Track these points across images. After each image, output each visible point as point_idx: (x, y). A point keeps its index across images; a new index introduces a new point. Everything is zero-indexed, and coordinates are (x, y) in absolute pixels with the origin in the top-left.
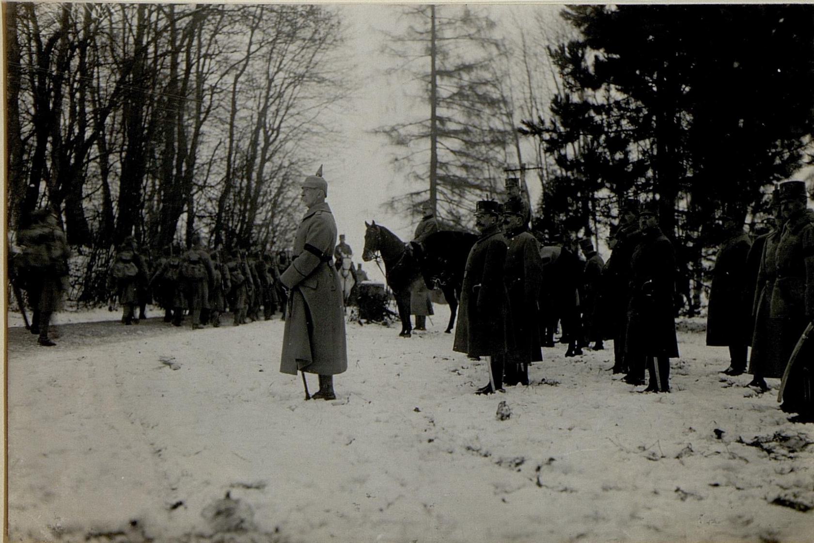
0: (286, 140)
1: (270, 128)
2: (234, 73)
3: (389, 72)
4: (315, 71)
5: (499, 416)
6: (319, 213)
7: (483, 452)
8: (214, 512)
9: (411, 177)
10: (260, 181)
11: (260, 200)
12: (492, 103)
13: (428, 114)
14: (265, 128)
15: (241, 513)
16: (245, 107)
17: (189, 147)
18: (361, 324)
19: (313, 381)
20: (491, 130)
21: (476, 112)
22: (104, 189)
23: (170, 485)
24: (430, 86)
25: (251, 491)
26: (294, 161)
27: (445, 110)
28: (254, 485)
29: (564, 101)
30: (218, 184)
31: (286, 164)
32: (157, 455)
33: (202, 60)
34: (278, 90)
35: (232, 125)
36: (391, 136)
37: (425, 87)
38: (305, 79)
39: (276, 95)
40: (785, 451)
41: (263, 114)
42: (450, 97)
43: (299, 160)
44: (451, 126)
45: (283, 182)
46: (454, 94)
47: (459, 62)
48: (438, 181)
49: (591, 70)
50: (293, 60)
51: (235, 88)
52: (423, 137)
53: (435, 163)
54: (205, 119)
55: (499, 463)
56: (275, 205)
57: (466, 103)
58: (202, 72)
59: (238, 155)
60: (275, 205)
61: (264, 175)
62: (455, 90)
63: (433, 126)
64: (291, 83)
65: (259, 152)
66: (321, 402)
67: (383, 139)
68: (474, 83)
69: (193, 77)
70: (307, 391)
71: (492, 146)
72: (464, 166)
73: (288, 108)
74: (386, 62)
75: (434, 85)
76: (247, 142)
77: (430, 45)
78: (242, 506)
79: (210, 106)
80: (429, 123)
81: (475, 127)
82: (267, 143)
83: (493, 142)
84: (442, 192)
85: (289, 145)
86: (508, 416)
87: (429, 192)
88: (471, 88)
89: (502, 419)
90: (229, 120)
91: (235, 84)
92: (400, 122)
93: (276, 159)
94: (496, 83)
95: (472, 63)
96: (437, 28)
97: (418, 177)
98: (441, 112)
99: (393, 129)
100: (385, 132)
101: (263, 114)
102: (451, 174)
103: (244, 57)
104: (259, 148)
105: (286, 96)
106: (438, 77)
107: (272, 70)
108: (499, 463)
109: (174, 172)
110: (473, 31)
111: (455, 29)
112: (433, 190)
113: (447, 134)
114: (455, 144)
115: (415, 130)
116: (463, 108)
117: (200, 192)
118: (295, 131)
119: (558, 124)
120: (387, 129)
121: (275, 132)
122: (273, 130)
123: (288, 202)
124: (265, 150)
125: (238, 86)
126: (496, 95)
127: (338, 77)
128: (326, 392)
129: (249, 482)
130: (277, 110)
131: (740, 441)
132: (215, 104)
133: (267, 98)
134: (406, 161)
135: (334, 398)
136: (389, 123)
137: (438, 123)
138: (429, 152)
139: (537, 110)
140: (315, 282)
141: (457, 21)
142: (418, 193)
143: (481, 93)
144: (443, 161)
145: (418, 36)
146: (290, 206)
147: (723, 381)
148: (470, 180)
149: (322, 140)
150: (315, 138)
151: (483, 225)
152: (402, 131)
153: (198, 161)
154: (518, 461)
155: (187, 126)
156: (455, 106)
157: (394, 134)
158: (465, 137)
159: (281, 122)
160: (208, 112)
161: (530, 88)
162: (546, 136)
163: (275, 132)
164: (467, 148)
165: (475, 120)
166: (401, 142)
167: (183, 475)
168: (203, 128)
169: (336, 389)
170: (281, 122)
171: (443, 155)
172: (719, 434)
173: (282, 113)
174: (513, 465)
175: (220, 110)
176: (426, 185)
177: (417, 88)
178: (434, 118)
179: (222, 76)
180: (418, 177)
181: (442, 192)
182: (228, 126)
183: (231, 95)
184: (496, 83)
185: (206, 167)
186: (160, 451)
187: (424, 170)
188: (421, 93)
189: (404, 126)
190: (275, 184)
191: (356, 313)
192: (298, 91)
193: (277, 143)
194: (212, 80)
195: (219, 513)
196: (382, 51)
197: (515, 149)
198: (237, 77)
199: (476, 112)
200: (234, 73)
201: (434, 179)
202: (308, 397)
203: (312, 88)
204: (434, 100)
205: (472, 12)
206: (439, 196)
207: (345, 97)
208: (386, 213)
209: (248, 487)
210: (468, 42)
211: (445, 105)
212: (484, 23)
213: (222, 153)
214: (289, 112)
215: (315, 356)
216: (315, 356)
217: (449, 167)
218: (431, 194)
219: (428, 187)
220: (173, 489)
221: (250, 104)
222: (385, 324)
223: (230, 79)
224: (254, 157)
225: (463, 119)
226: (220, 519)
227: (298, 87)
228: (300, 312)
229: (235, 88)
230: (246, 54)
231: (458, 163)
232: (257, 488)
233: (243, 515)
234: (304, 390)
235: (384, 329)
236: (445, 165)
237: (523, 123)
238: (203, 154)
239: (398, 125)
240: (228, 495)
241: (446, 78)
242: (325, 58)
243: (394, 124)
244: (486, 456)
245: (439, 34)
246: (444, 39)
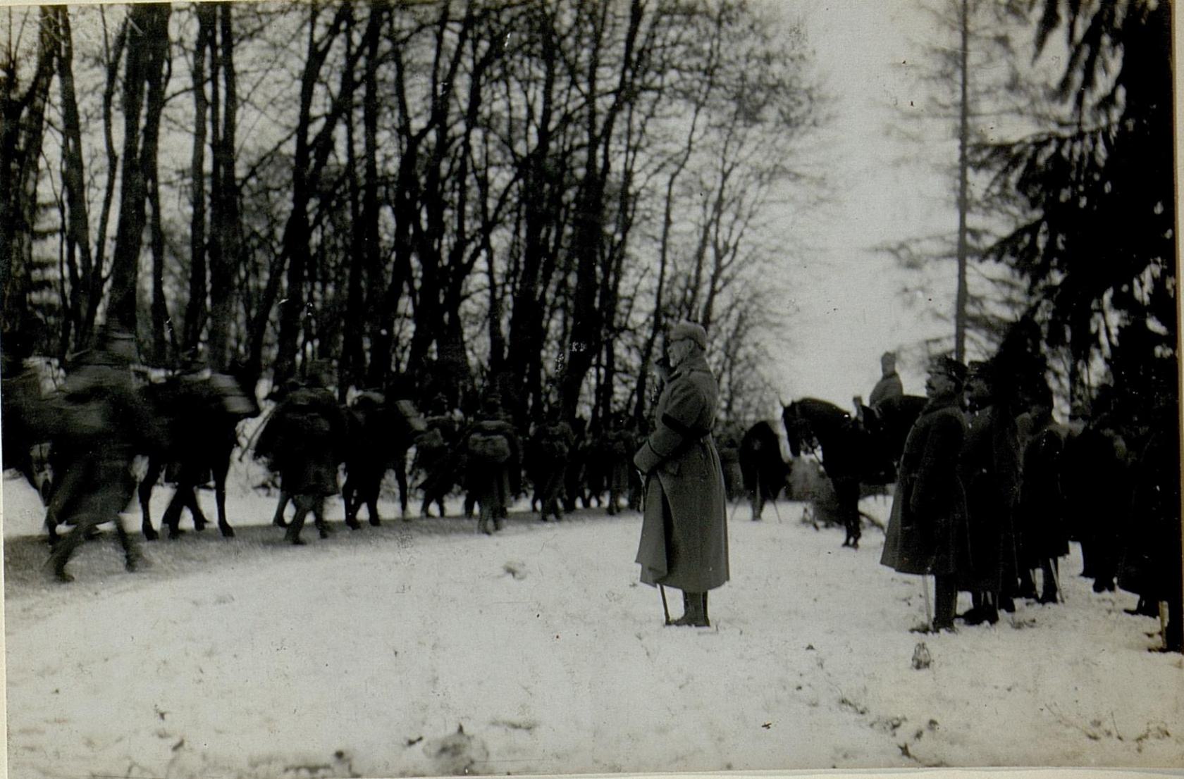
3: (897, 163)
7: (860, 708)
8: (439, 747)
9: (928, 316)
15: (473, 752)
18: (816, 527)
19: (676, 599)
24: (958, 183)
25: (518, 731)
36: (898, 257)
37: (951, 186)
48: (969, 323)
53: (963, 296)
63: (962, 244)
66: (690, 632)
67: (889, 260)
74: (890, 149)
77: (959, 122)
78: (475, 744)
80: (955, 238)
82: (719, 269)
84: (972, 339)
89: (918, 667)
91: (670, 184)
96: (970, 98)
97: (938, 316)
98: (974, 221)
99: (902, 246)
102: (986, 313)
105: (747, 201)
106: (970, 171)
110: (1023, 103)
111: (997, 100)
112: (960, 338)
115: (936, 248)
120: (894, 246)
124: (714, 279)
128: (696, 614)
134: (920, 294)
137: (968, 237)
140: (677, 466)
141: (999, 87)
142: (937, 341)
145: (942, 111)
152: (915, 249)
156: (995, 212)
157: (903, 253)
166: (913, 265)
169: (712, 610)
171: (976, 284)
174: (888, 728)
176: (950, 329)
178: (963, 229)
180: (938, 316)
181: (972, 339)
187: (947, 306)
188: (945, 194)
189: (918, 241)
191: (811, 512)
195: (444, 750)
196: (887, 134)
201: (963, 321)
202: (668, 623)
203: (784, 187)
204: (964, 205)
205: (1022, 76)
210: (1015, 119)
211: (981, 210)
212: (1041, 91)
226: (445, 757)
228: (656, 506)
230: (686, 145)
232: (528, 728)
233: (474, 755)
236: (978, 300)
239: (910, 240)
240: (461, 729)
243: (902, 238)
244: (862, 713)
245: (972, 108)
246: (980, 115)
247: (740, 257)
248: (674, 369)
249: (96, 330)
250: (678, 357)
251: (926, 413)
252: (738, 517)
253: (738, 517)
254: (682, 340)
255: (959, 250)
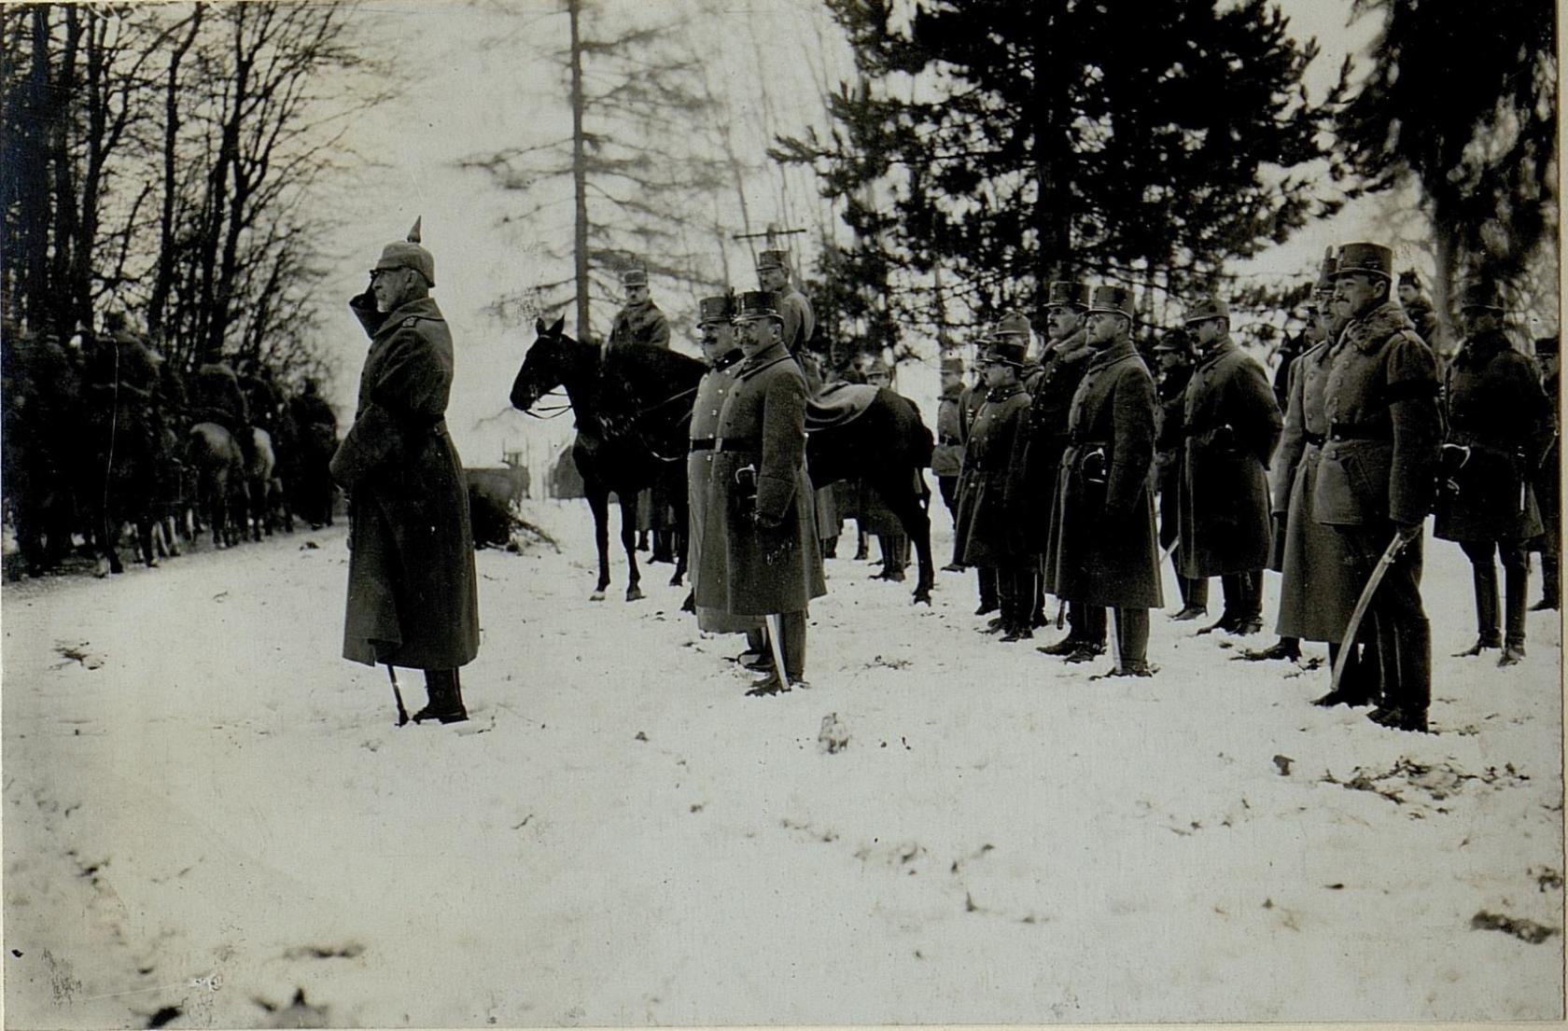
0: (279, 183)
1: (247, 159)
2: (169, 47)
3: (485, 46)
4: (339, 41)
5: (826, 744)
6: (410, 322)
10: (231, 267)
11: (233, 305)
12: (694, 106)
13: (570, 131)
14: (236, 158)
16: (193, 117)
17: (80, 198)
19: (414, 685)
20: (691, 161)
21: (663, 125)
22: (100, 165)
23: (136, 959)
24: (569, 74)
26: (298, 225)
27: (601, 119)
28: (337, 950)
29: (858, 98)
30: (148, 273)
31: (282, 232)
32: (88, 879)
33: (99, 23)
34: (261, 83)
35: (169, 152)
38: (317, 59)
39: (260, 91)
40: (1426, 796)
41: (231, 132)
42: (610, 96)
43: (309, 223)
44: (611, 153)
45: (276, 271)
46: (618, 90)
47: (625, 26)
48: (592, 262)
49: (907, 33)
50: (289, 21)
51: (173, 78)
52: (558, 173)
54: (113, 143)
55: (862, 855)
56: (263, 316)
57: (640, 106)
58: (101, 48)
59: (186, 215)
60: (263, 316)
61: (238, 254)
62: (621, 81)
63: (578, 155)
64: (285, 70)
65: (228, 209)
67: (480, 178)
68: (655, 67)
69: (82, 57)
70: (400, 706)
71: (696, 190)
72: (642, 231)
73: (282, 119)
75: (578, 72)
76: (202, 189)
79: (123, 115)
80: (570, 146)
81: (659, 153)
83: (696, 184)
85: (286, 194)
86: (844, 744)
87: (574, 283)
88: (651, 76)
90: (162, 145)
91: (173, 69)
92: (513, 146)
93: (260, 220)
94: (696, 65)
95: (651, 27)
98: (591, 124)
99: (498, 160)
100: (481, 165)
101: (231, 132)
102: (615, 247)
103: (190, 14)
104: (226, 200)
106: (584, 55)
107: (249, 40)
108: (862, 855)
109: (51, 252)
113: (606, 168)
114: (622, 186)
115: (547, 161)
116: (636, 117)
117: (110, 292)
118: (300, 165)
119: (847, 143)
120: (487, 159)
121: (259, 167)
122: (254, 164)
123: (287, 311)
124: (237, 204)
125: (180, 72)
126: (696, 89)
127: (384, 56)
128: (446, 705)
129: (323, 945)
130: (262, 123)
131: (1330, 780)
132: (134, 110)
133: (241, 97)
134: (526, 223)
135: (463, 717)
136: (489, 145)
137: (586, 144)
138: (573, 203)
139: (776, 121)
142: (551, 287)
143: (669, 88)
144: (600, 223)
146: (293, 316)
147: (1226, 646)
148: (654, 259)
149: (354, 181)
150: (342, 178)
151: (756, 343)
152: (516, 163)
153: (100, 229)
154: (906, 852)
155: (76, 157)
157: (501, 168)
158: (642, 175)
159: (269, 147)
160: (118, 127)
161: (761, 78)
162: (824, 165)
163: (259, 167)
164: (647, 196)
165: (657, 140)
166: (514, 185)
167: (163, 935)
168: (111, 161)
169: (468, 699)
170: (269, 147)
171: (599, 212)
172: (1283, 764)
173: (269, 129)
174: (897, 860)
175: (144, 123)
176: (569, 269)
177: (548, 78)
178: (580, 136)
179: (146, 53)
182: (160, 157)
183: (165, 94)
184: (696, 65)
185: (121, 240)
186: (92, 870)
187: (563, 240)
190: (262, 274)
192: (307, 84)
193: (261, 190)
194: (123, 64)
197: (735, 198)
198: (177, 56)
199: (663, 125)
200: (169, 47)
201: (583, 259)
202: (403, 719)
204: (578, 102)
206: (593, 290)
207: (399, 94)
208: (490, 325)
209: (323, 954)
213: (153, 209)
214: (285, 126)
215: (416, 624)
216: (416, 624)
217: (612, 233)
218: (579, 288)
219: (573, 274)
220: (145, 972)
221: (204, 109)
222: (514, 548)
223: (163, 58)
224: (219, 219)
225: (637, 139)
227: (303, 76)
229: (173, 78)
231: (632, 227)
232: (344, 954)
234: (395, 702)
235: (512, 557)
237: (779, 139)
238: (112, 215)
239: (508, 150)
241: (600, 57)
242: (358, 17)
243: (497, 149)
247: (272, 176)
248: (385, 316)
249: (1053, 560)
250: (391, 297)
251: (1284, 407)
252: (476, 553)
253: (476, 553)
254: (398, 269)
255: (576, 163)
